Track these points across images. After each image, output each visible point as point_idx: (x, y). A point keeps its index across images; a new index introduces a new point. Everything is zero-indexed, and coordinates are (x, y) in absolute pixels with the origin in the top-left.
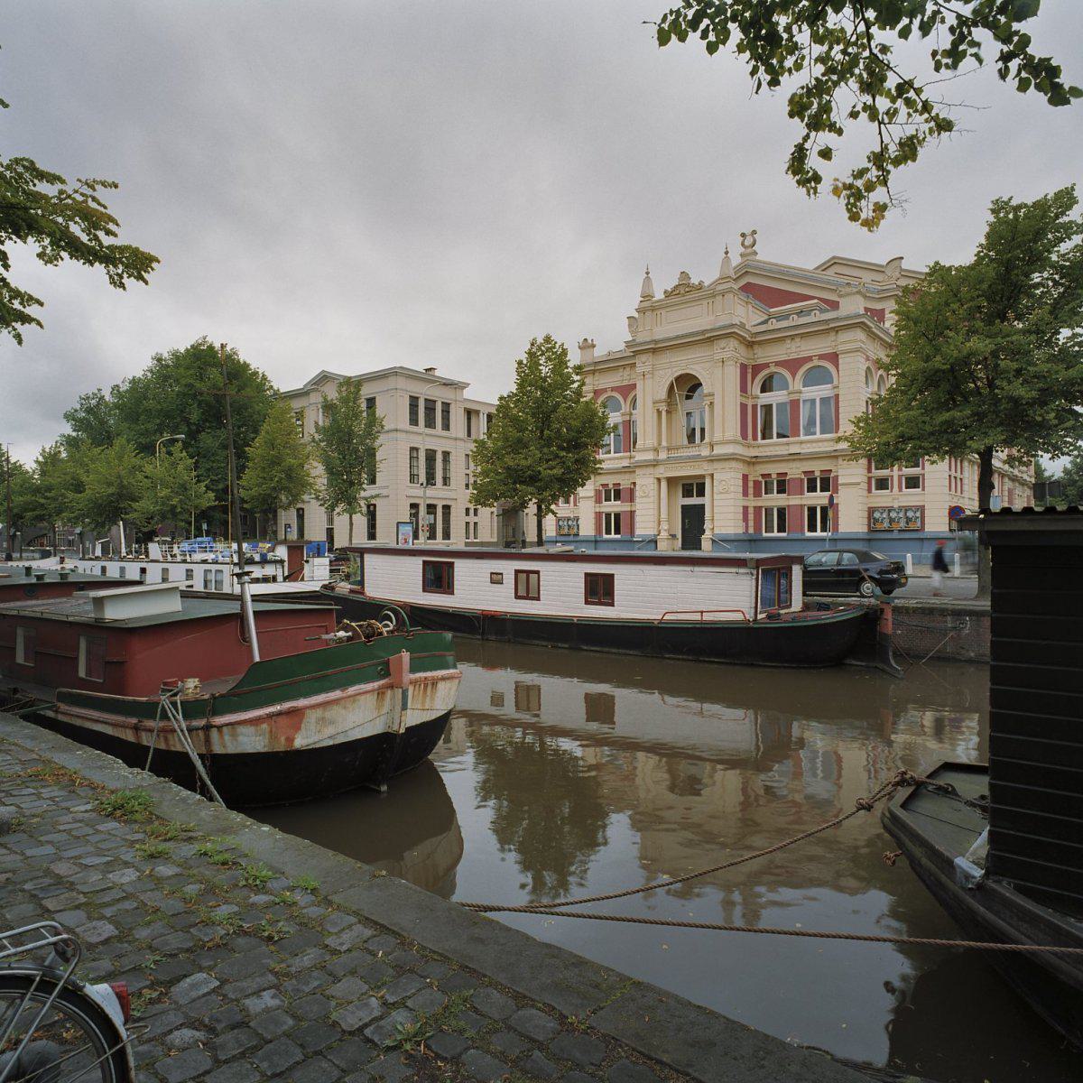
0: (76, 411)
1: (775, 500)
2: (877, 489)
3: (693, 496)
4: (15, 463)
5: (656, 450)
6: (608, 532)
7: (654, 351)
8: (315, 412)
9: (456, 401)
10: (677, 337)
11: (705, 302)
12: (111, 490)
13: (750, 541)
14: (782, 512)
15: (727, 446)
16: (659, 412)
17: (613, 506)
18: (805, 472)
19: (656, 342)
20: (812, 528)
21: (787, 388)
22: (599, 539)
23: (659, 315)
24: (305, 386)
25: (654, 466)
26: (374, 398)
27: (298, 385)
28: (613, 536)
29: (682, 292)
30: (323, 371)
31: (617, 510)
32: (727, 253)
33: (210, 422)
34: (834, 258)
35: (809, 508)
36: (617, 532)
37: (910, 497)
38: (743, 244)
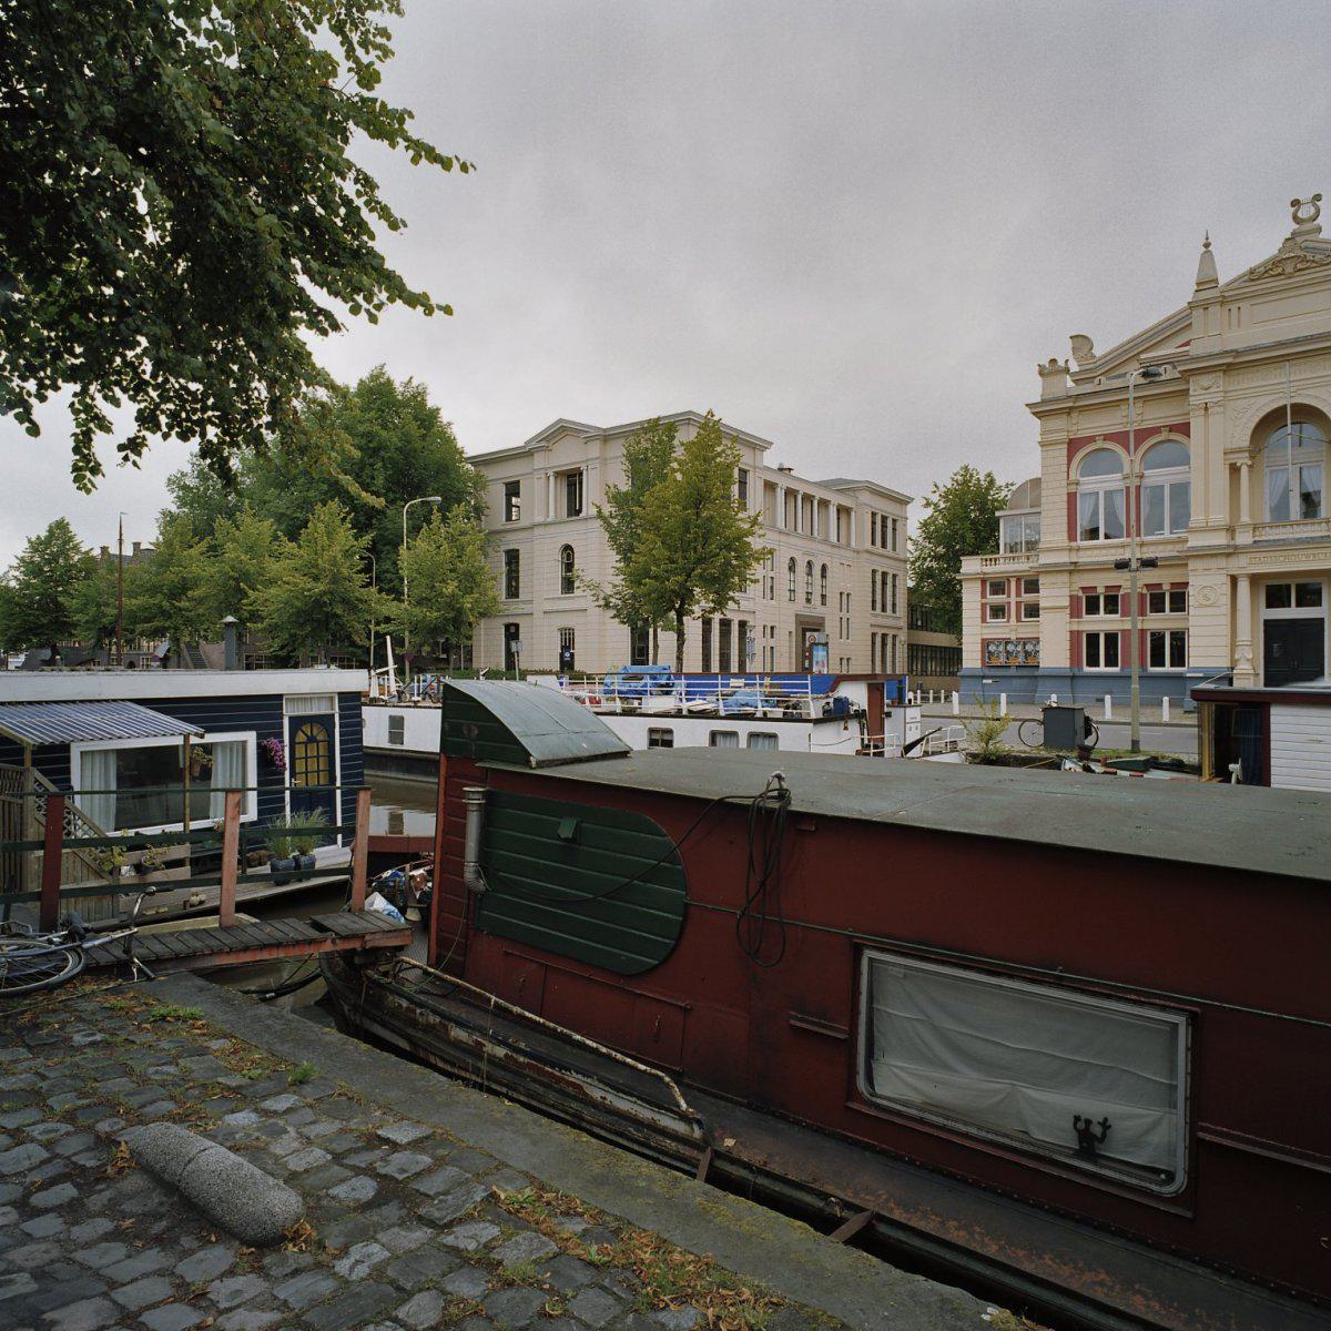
0: (183, 475)
1: (1102, 622)
2: (1087, 613)
3: (1289, 606)
4: (87, 553)
5: (1231, 530)
6: (1093, 661)
7: (1228, 369)
8: (543, 481)
9: (755, 467)
10: (1296, 342)
12: (320, 587)
14: (1111, 638)
15: (1057, 554)
16: (1234, 470)
18: (1147, 586)
19: (1237, 353)
20: (1093, 661)
21: (1120, 469)
22: (1077, 674)
23: (1234, 310)
24: (527, 443)
25: (1228, 555)
26: (519, 481)
27: (516, 437)
28: (1102, 669)
29: (1289, 270)
30: (560, 420)
32: (1207, 245)
33: (394, 492)
35: (1153, 634)
36: (1111, 661)
37: (1025, 629)
38: (1295, 218)
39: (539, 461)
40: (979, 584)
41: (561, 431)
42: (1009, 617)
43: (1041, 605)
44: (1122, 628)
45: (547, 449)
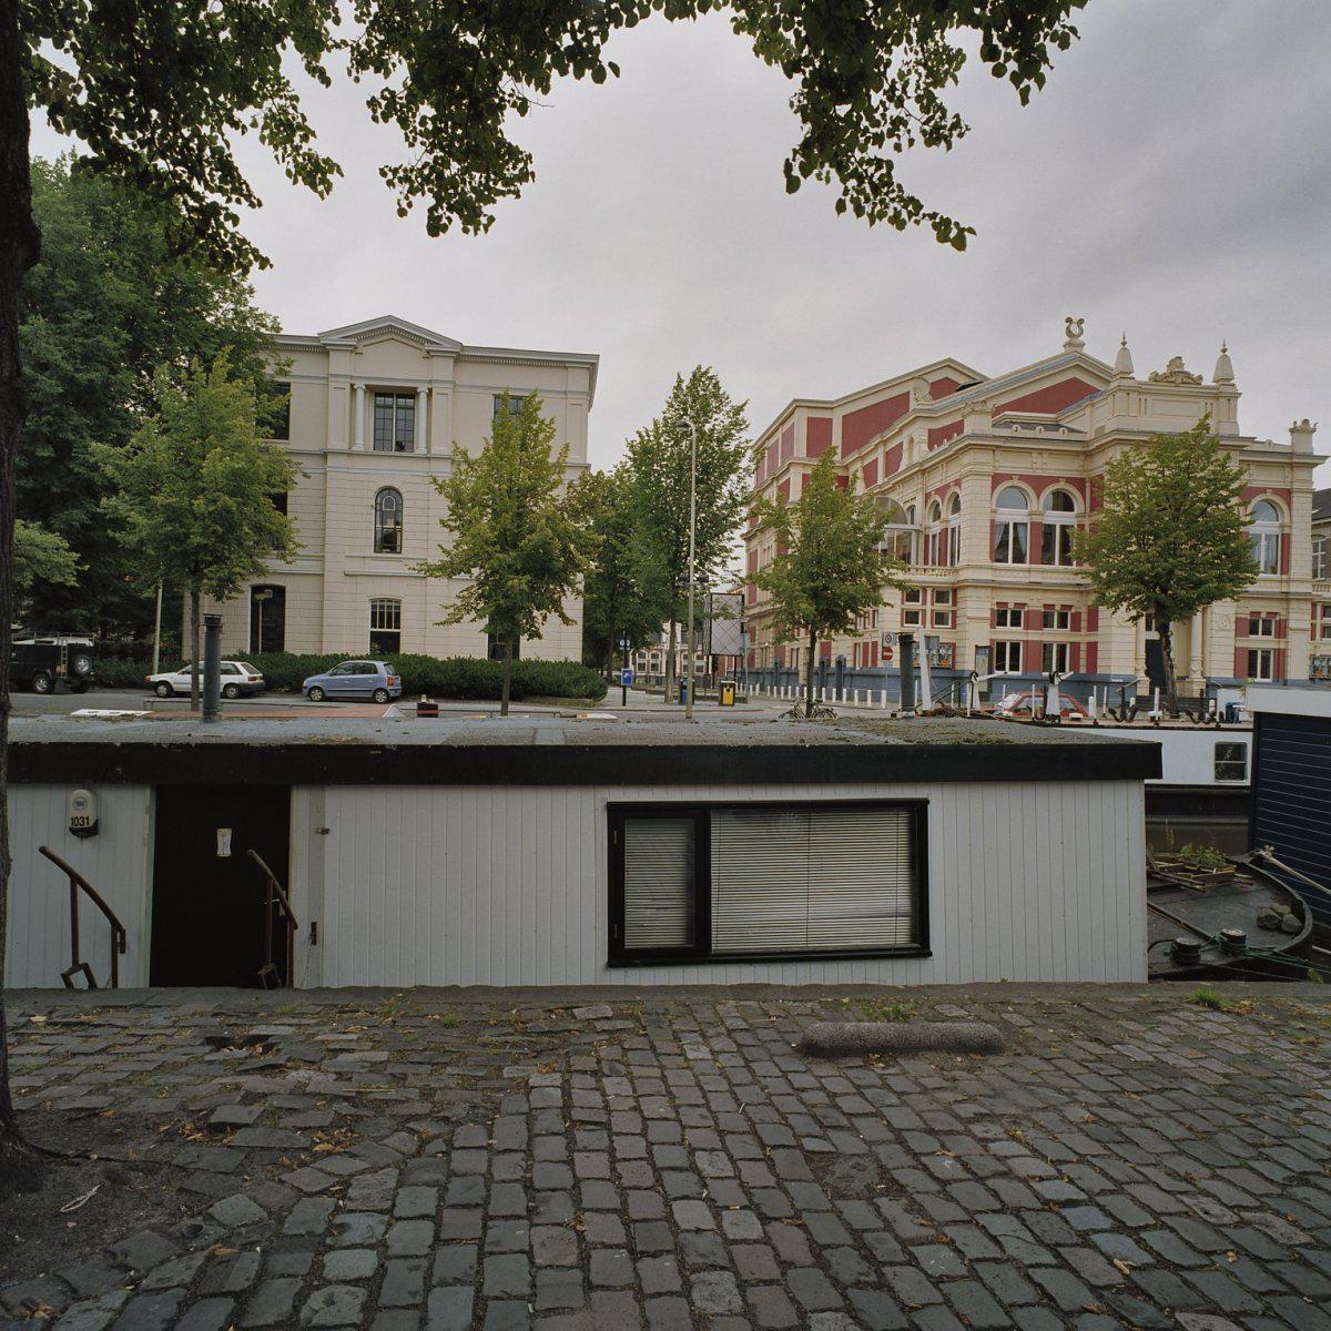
1: (1009, 633)
13: (1079, 682)
14: (1015, 647)
17: (1260, 642)
28: (1258, 679)
30: (390, 318)
31: (1062, 639)
32: (1124, 343)
34: (950, 360)
36: (1014, 667)
39: (339, 363)
40: (1309, 606)
41: (389, 331)
42: (924, 623)
45: (354, 350)
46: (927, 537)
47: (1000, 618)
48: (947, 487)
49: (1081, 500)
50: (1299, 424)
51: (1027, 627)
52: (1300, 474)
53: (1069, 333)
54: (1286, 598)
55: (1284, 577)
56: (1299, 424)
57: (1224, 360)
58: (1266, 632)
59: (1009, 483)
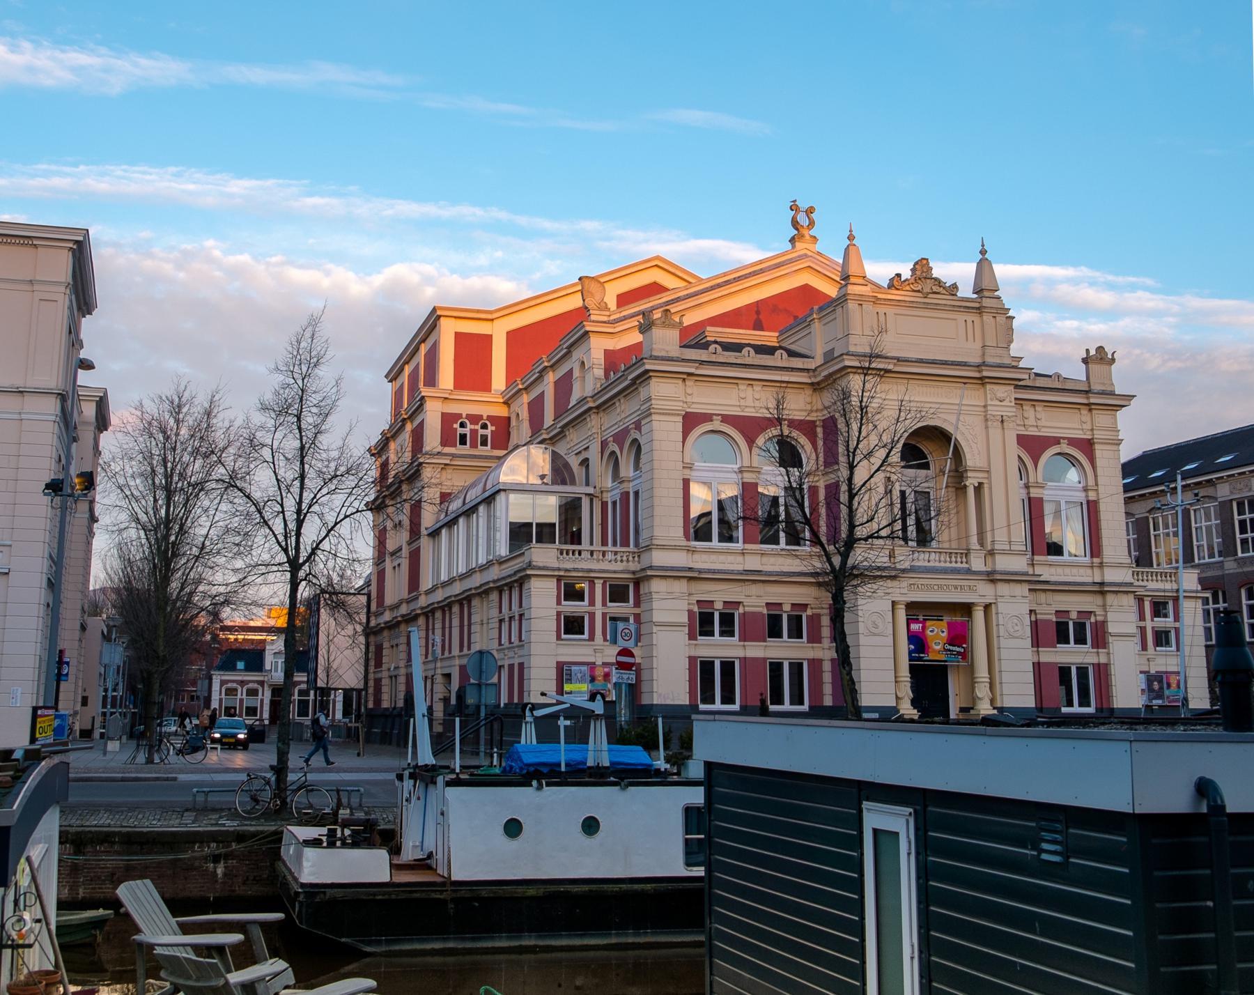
1: (719, 647)
11: (961, 317)
14: (728, 667)
17: (1072, 655)
28: (718, 706)
43: (1111, 628)
44: (741, 654)
46: (604, 505)
47: (703, 623)
48: (626, 431)
49: (808, 447)
50: (1093, 352)
51: (743, 638)
52: (1102, 419)
53: (795, 224)
54: (1101, 589)
55: (1096, 560)
56: (1093, 352)
57: (984, 266)
58: (1081, 640)
59: (1055, 449)
